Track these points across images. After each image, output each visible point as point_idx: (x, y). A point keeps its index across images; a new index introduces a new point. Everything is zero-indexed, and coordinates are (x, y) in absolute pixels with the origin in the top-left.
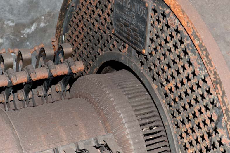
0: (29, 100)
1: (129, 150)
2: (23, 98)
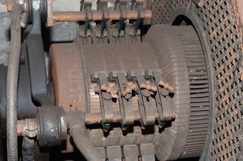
0: (104, 38)
1: (174, 85)
2: (99, 36)
